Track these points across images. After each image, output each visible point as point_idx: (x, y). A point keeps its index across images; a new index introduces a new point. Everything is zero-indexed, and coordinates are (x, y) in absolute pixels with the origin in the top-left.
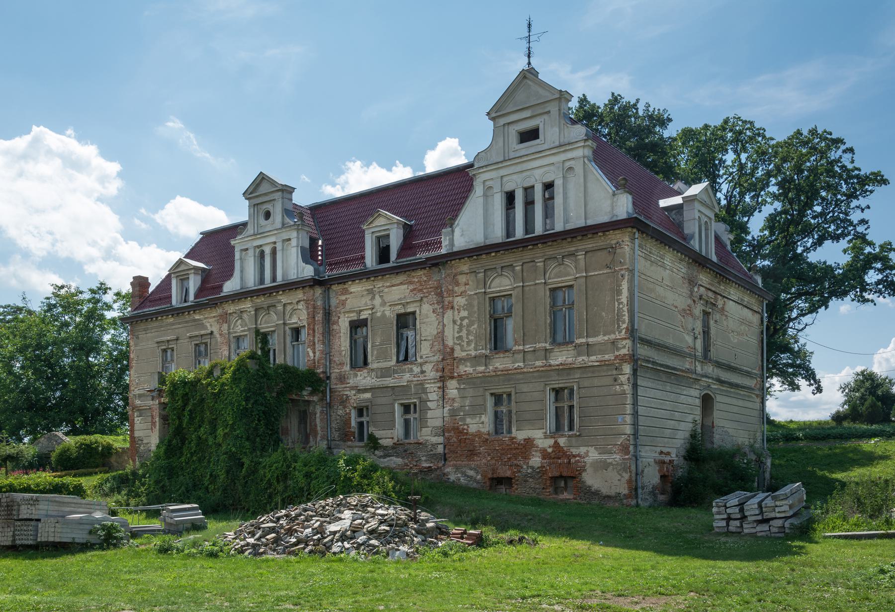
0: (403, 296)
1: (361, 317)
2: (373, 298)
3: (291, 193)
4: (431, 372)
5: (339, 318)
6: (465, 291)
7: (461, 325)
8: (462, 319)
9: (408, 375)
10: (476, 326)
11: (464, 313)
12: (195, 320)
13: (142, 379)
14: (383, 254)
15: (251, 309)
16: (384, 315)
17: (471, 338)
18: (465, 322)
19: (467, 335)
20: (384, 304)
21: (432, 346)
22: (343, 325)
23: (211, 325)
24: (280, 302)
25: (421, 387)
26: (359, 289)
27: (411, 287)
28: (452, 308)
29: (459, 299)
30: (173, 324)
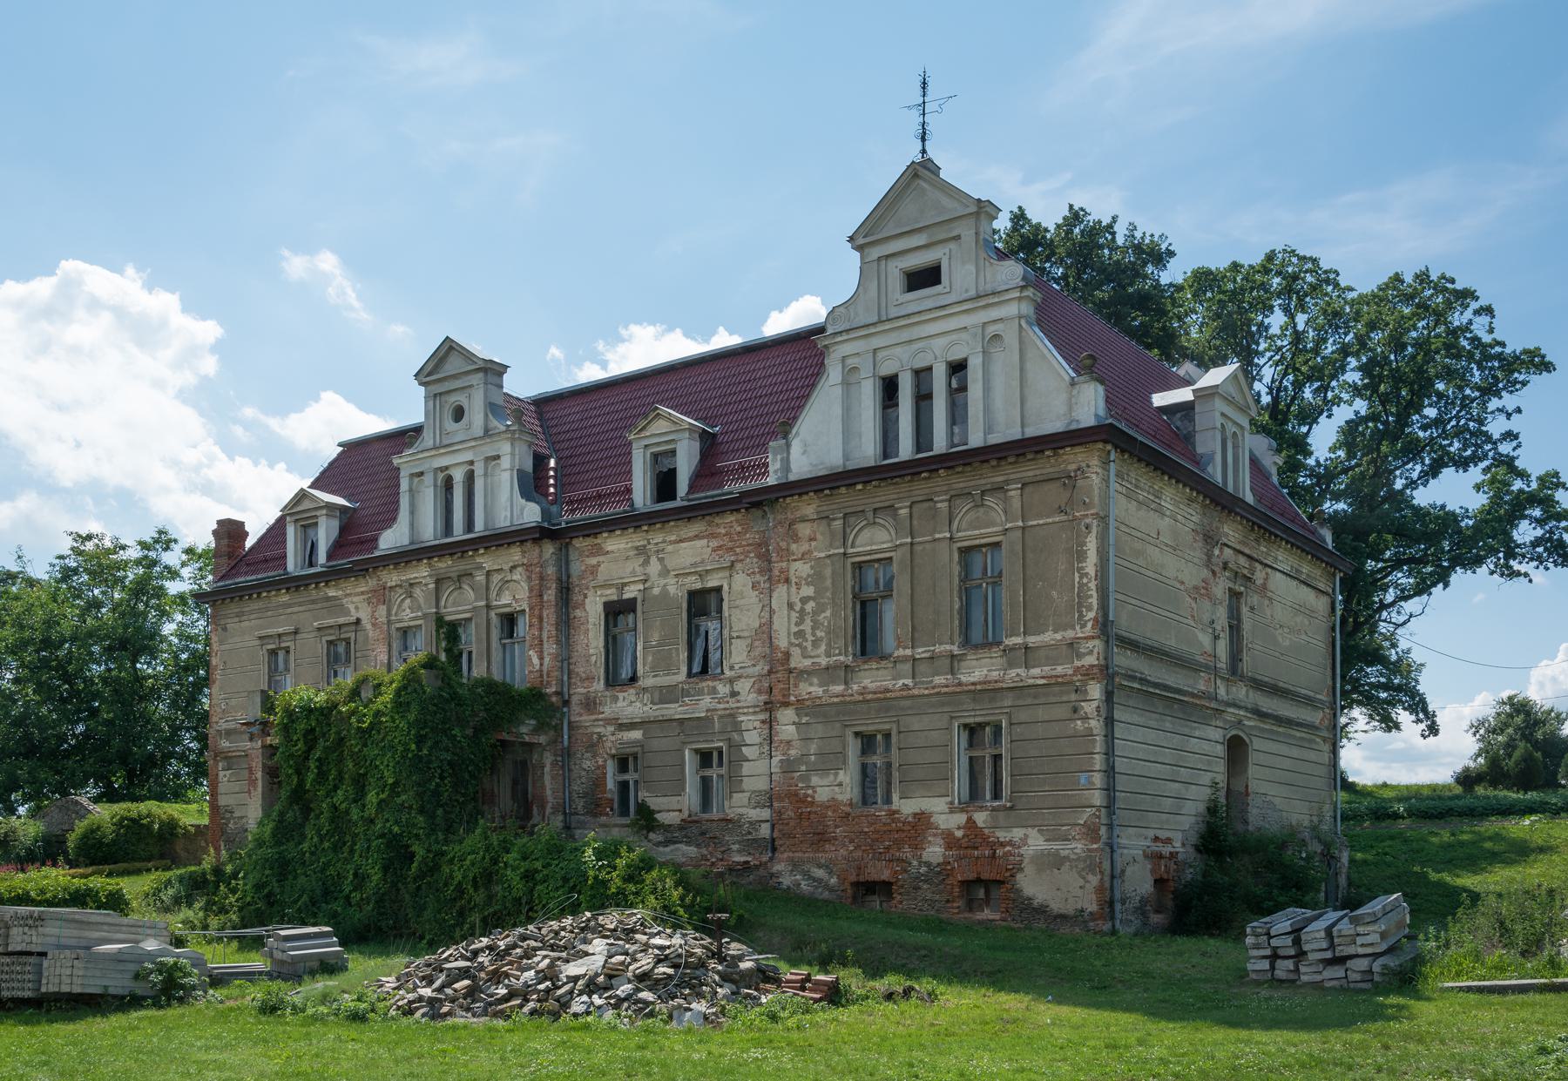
0: (698, 559)
1: (625, 596)
2: (646, 562)
6: (810, 552)
7: (802, 610)
8: (804, 600)
9: (708, 699)
11: (808, 591)
12: (328, 599)
14: (665, 484)
17: (820, 634)
18: (810, 606)
19: (813, 628)
20: (665, 572)
21: (751, 648)
22: (592, 609)
24: (480, 567)
27: (714, 543)
28: (787, 581)
29: (798, 565)
30: (290, 606)
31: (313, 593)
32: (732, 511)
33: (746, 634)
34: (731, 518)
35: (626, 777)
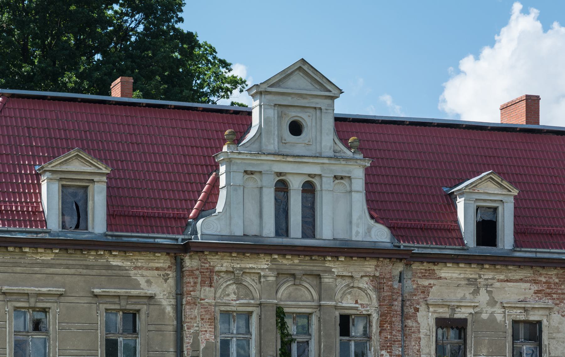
0: (522, 298)
1: (457, 316)
2: (476, 292)
5: (417, 310)
12: (109, 267)
14: (487, 231)
15: (268, 272)
20: (492, 302)
22: (425, 321)
23: (148, 282)
24: (330, 271)
26: (455, 275)
27: (535, 287)
30: (51, 266)
31: (91, 258)
34: (553, 272)
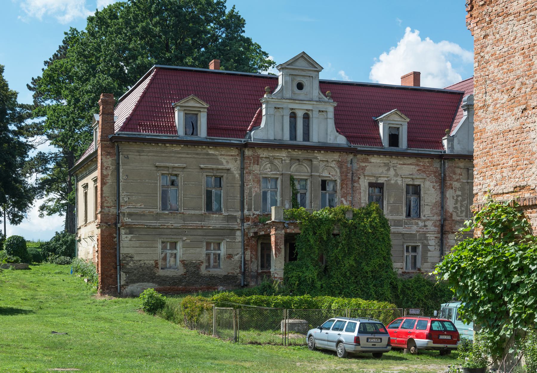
0: (411, 173)
1: (379, 182)
2: (388, 170)
3: (318, 71)
4: (432, 228)
5: (359, 178)
6: (459, 179)
7: (457, 200)
8: (458, 196)
9: (415, 227)
10: (466, 202)
11: (459, 193)
12: (208, 154)
13: (134, 198)
14: (394, 139)
16: (396, 183)
17: (463, 209)
18: (460, 198)
19: (461, 207)
20: (396, 175)
21: (432, 210)
23: (227, 162)
25: (424, 237)
26: (378, 161)
27: (418, 168)
28: (452, 188)
29: (455, 183)
30: (179, 153)
32: (431, 158)
33: (430, 204)
35: (414, 254)
